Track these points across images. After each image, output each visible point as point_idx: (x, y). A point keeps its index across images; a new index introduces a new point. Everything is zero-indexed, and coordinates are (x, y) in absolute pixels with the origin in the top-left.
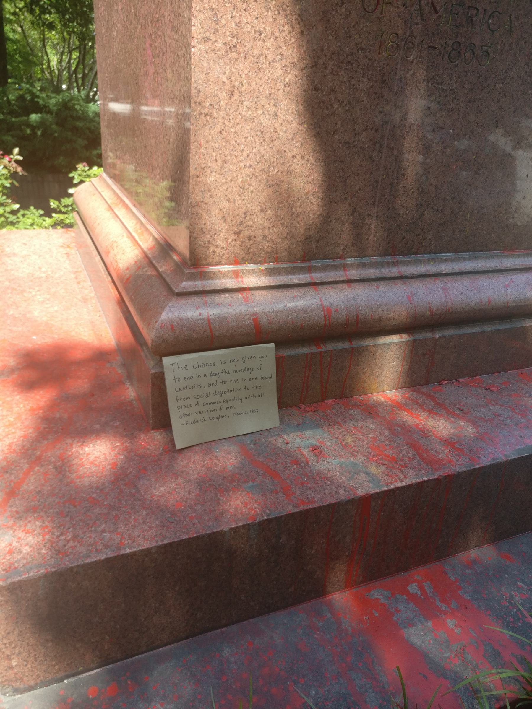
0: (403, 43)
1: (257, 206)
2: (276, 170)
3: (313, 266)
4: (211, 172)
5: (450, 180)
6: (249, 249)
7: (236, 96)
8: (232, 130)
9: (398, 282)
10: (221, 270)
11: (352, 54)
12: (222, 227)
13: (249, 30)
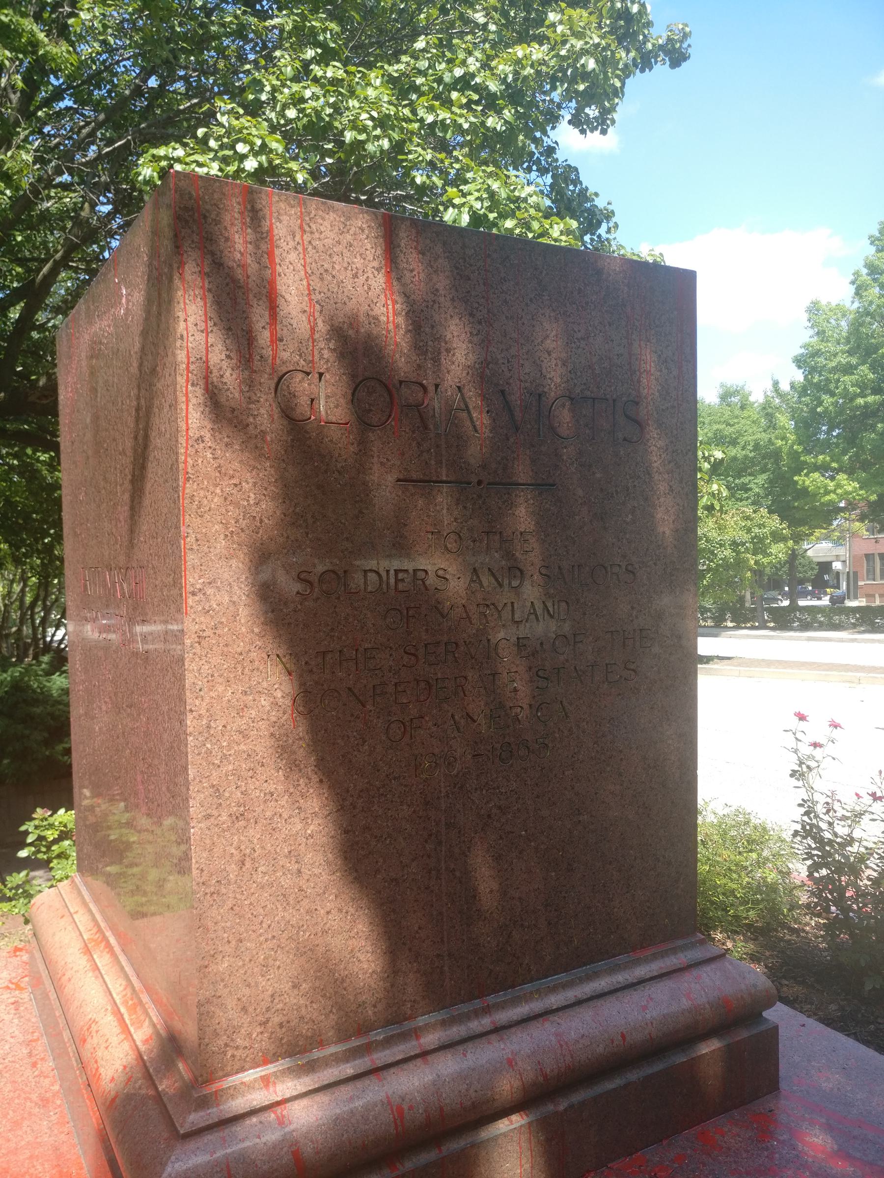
0: (442, 760)
1: (288, 982)
2: (308, 934)
3: (372, 1042)
4: (223, 957)
5: (536, 887)
6: (282, 1039)
7: (248, 865)
8: (246, 902)
9: (493, 1037)
10: (244, 1080)
11: (384, 786)
12: (243, 1021)
13: (257, 794)
